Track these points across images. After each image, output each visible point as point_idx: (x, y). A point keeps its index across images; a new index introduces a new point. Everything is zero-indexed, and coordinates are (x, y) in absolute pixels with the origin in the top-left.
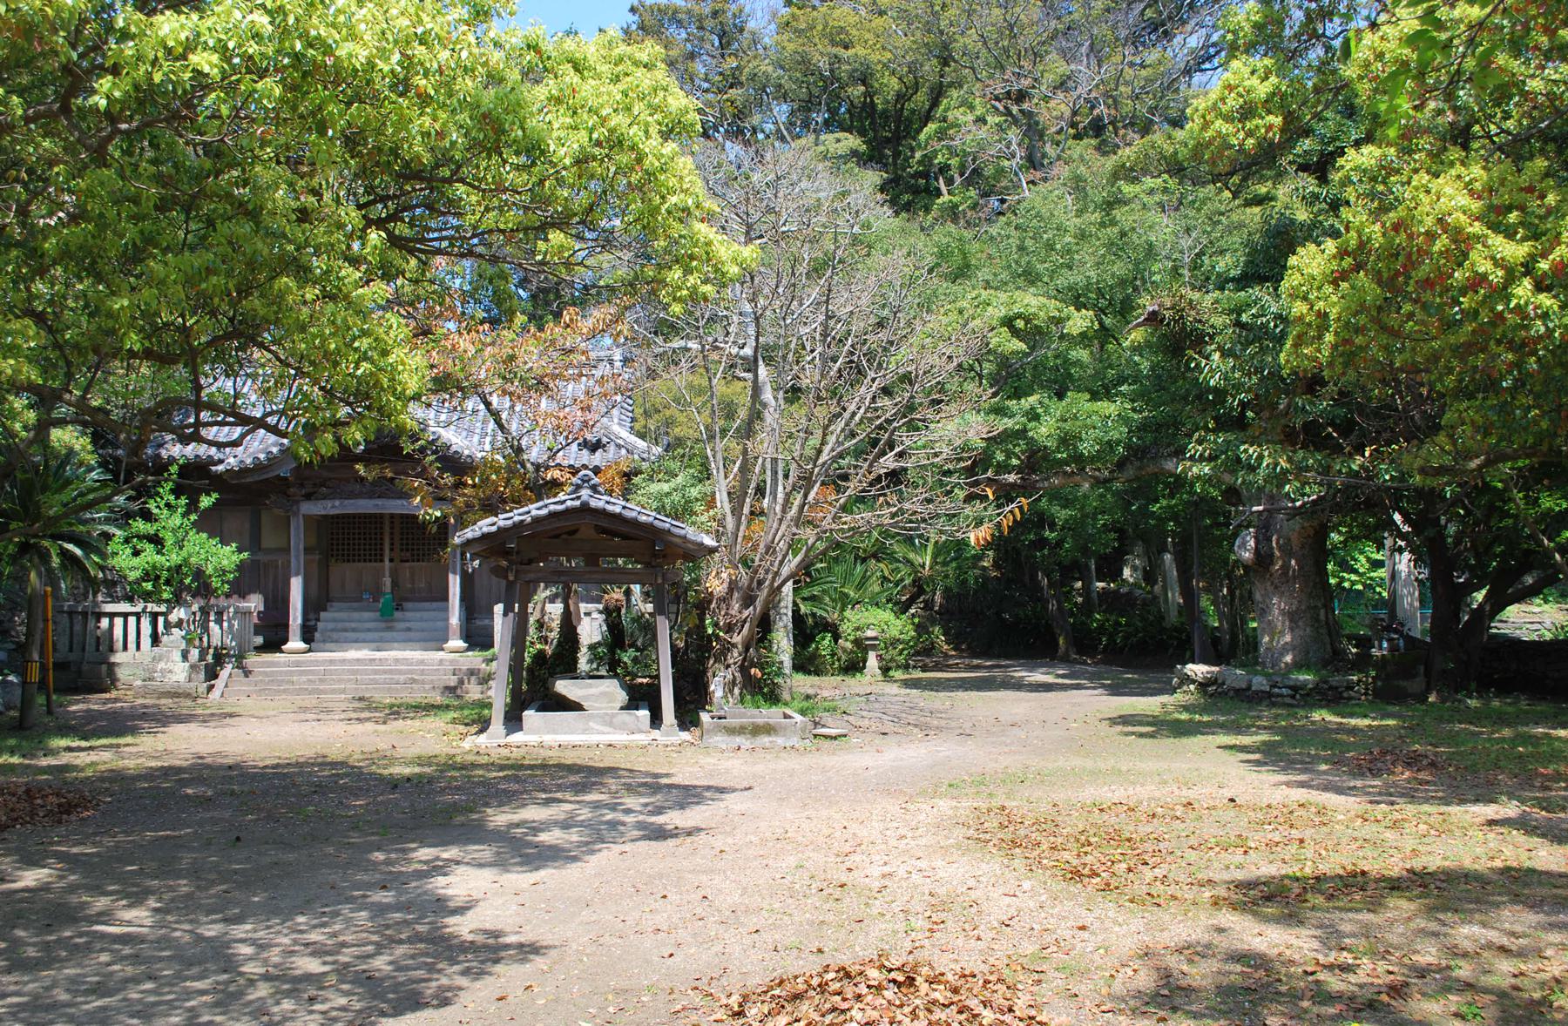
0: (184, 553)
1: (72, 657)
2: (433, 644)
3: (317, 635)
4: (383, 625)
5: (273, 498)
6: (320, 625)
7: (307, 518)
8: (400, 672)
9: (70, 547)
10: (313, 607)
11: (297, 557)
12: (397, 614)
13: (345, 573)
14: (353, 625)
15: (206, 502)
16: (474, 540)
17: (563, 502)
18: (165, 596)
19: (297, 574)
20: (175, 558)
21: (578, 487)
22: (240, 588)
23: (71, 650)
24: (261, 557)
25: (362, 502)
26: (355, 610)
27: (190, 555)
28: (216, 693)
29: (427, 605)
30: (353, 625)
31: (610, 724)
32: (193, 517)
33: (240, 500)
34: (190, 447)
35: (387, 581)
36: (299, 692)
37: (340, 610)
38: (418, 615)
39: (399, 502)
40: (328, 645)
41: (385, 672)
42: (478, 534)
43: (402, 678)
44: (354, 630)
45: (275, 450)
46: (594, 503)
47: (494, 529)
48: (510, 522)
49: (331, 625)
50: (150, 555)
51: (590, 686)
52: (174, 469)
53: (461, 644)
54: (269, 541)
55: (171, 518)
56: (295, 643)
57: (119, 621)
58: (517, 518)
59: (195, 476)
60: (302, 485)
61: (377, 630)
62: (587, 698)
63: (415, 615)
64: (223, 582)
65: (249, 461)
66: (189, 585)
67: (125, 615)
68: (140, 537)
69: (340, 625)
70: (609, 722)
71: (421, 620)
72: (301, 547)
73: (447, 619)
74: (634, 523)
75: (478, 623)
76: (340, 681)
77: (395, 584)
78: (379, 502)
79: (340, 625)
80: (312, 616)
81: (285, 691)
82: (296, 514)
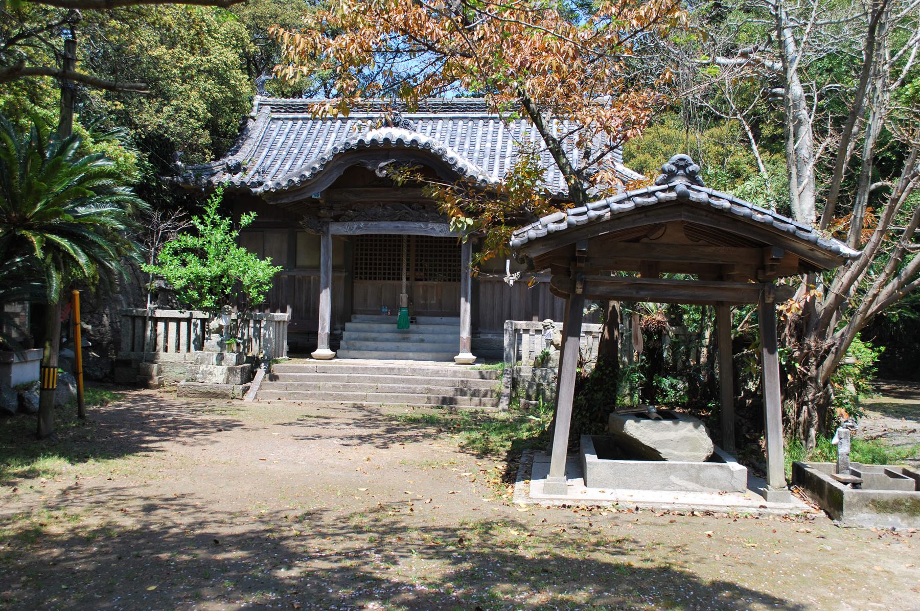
0: (223, 265)
1: (133, 355)
2: (444, 355)
3: (342, 343)
4: (399, 336)
5: (306, 219)
6: (345, 334)
7: (334, 236)
8: (417, 382)
9: (56, 238)
10: (339, 318)
11: (326, 273)
12: (413, 327)
13: (367, 289)
14: (374, 335)
15: (246, 220)
16: (538, 240)
17: (653, 193)
18: (206, 304)
19: (325, 288)
20: (214, 269)
21: (671, 175)
22: (273, 303)
23: (133, 350)
24: (298, 274)
25: (383, 224)
26: (374, 321)
27: (229, 267)
28: (250, 395)
29: (437, 319)
30: (374, 335)
31: (697, 480)
32: (235, 234)
33: (274, 217)
34: (238, 176)
35: (404, 297)
36: (324, 397)
37: (363, 321)
38: (430, 328)
39: (417, 224)
40: (352, 353)
41: (403, 381)
42: (542, 232)
43: (419, 387)
44: (374, 340)
45: (307, 174)
46: (694, 196)
47: (563, 226)
48: (584, 218)
49: (354, 335)
50: (195, 267)
51: (668, 429)
52: (220, 191)
53: (470, 356)
54: (303, 260)
55: (216, 233)
56: (323, 350)
57: (161, 326)
58: (592, 214)
59: (237, 200)
60: (331, 208)
61: (394, 340)
62: (664, 443)
63: (428, 328)
64: (259, 293)
65: (284, 184)
66: (228, 294)
67: (178, 321)
68: (187, 250)
69: (363, 335)
70: (696, 478)
71: (433, 333)
72: (330, 263)
73: (459, 333)
74: (747, 222)
75: (483, 337)
76: (361, 388)
77: (410, 300)
78: (399, 224)
79: (363, 335)
80: (338, 326)
81: (311, 396)
82: (326, 234)
